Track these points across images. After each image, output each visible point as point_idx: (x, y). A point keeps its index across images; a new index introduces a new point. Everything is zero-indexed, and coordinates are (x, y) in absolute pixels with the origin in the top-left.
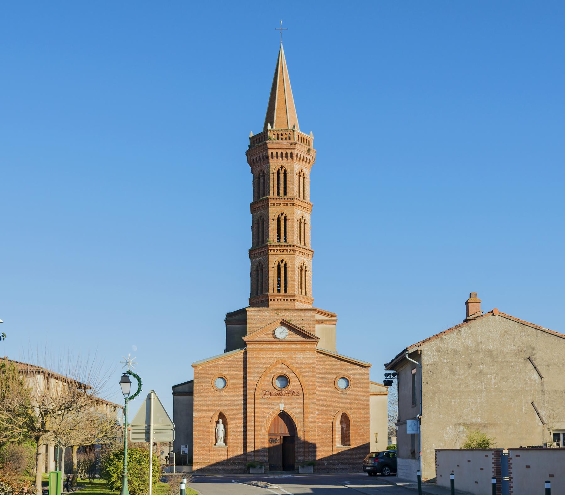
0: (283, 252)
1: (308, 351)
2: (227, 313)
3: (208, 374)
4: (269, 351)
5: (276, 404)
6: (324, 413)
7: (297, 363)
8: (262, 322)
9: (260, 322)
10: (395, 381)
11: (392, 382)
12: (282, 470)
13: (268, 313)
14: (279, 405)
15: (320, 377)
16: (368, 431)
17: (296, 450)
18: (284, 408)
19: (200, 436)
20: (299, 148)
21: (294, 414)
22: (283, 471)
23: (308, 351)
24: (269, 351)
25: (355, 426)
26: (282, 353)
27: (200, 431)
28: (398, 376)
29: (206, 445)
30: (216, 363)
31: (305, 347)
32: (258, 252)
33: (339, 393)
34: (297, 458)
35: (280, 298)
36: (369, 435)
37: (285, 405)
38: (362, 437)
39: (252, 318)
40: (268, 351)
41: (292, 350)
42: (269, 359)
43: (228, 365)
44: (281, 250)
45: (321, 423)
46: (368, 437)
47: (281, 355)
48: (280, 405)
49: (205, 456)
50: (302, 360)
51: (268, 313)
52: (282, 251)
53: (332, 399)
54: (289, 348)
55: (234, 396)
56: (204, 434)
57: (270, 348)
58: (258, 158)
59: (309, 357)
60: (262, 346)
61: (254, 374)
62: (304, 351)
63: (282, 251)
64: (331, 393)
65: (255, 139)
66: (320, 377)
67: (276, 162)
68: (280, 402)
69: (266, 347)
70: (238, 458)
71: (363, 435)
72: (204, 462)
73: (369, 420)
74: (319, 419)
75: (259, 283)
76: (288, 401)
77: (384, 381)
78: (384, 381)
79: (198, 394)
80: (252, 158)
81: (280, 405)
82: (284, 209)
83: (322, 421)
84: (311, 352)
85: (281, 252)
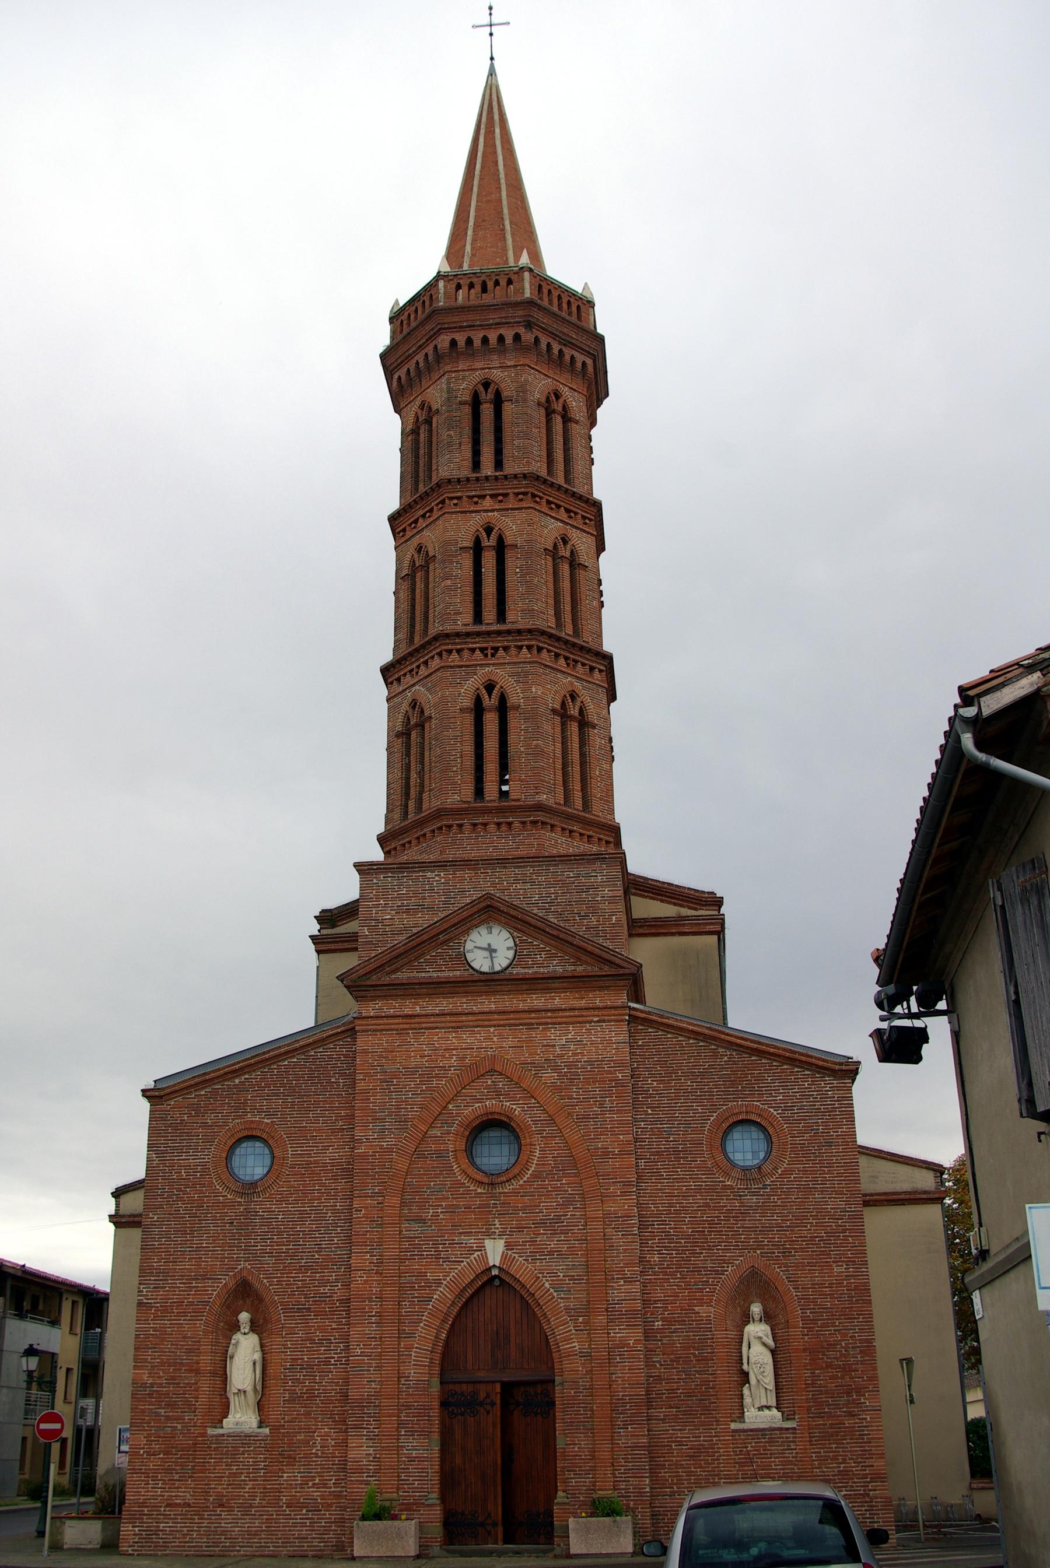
0: (493, 655)
1: (596, 1019)
2: (323, 911)
3: (205, 1125)
4: (443, 1025)
5: (471, 1241)
6: (673, 1274)
7: (555, 1068)
8: (416, 911)
9: (408, 911)
10: (939, 1028)
11: (922, 1036)
12: (500, 1536)
13: (437, 878)
14: (481, 1248)
15: (652, 1123)
16: (868, 1349)
17: (560, 1443)
18: (504, 1257)
19: (160, 1385)
20: (543, 323)
21: (547, 1285)
22: (505, 1543)
23: (596, 1019)
24: (443, 1025)
25: (810, 1329)
26: (492, 1030)
27: (162, 1363)
28: (951, 1003)
29: (179, 1426)
30: (237, 1081)
31: (583, 1003)
32: (409, 668)
33: (731, 1187)
34: (565, 1481)
35: (486, 819)
36: (875, 1369)
37: (508, 1246)
38: (842, 1377)
39: (378, 899)
40: (439, 1025)
41: (533, 1015)
42: (444, 1056)
43: (283, 1085)
44: (486, 649)
45: (663, 1319)
46: (870, 1379)
47: (488, 1038)
48: (488, 1243)
49: (176, 1477)
50: (574, 1054)
51: (437, 878)
52: (489, 652)
53: (704, 1212)
54: (521, 1006)
55: (302, 1212)
56: (173, 1378)
57: (446, 1010)
58: (411, 371)
59: (603, 1039)
60: (416, 1004)
61: (383, 1120)
62: (578, 1017)
63: (489, 652)
64: (699, 1189)
65: (404, 317)
66: (652, 1123)
67: (468, 370)
68: (490, 1234)
69: (430, 1009)
70: (310, 1484)
71: (847, 1369)
72: (168, 1505)
73: (870, 1302)
74: (655, 1302)
75: (414, 775)
76: (520, 1229)
77: (878, 1034)
78: (878, 1034)
79: (161, 1207)
80: (396, 376)
81: (488, 1243)
82: (496, 513)
83: (665, 1309)
84: (609, 1021)
85: (486, 655)
